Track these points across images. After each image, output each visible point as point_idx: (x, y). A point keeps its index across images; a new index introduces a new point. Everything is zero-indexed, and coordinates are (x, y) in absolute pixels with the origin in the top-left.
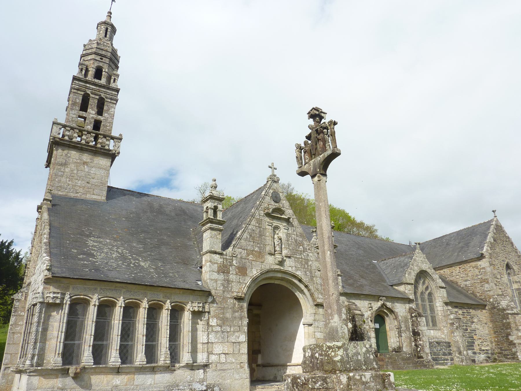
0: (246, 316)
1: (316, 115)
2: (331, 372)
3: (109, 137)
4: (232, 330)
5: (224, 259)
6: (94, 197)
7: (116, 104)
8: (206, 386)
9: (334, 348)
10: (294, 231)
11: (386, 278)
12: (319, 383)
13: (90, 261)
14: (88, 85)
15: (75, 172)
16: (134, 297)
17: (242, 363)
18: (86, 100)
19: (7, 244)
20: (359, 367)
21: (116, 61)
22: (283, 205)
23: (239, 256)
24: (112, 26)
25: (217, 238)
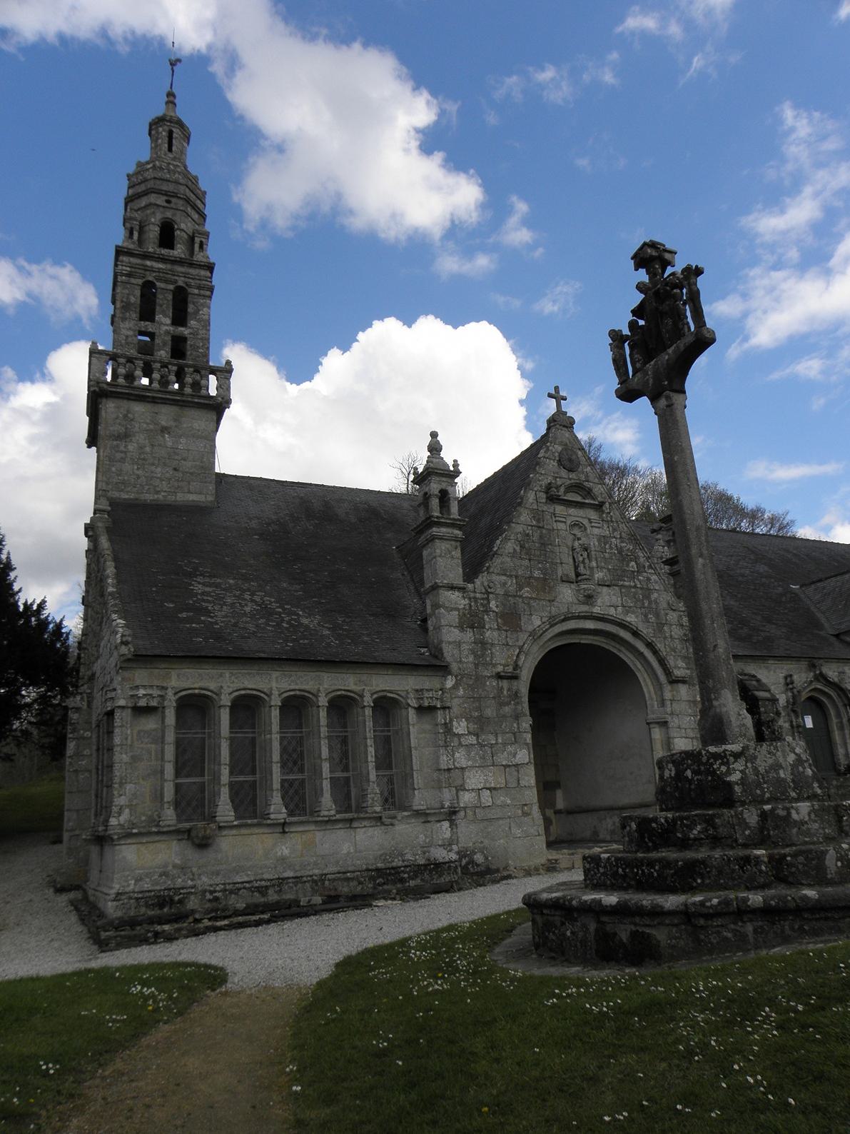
0: (528, 714)
1: (651, 257)
2: (721, 806)
3: (206, 369)
4: (500, 741)
5: (470, 599)
6: (192, 497)
7: (210, 297)
8: (458, 853)
9: (725, 756)
10: (614, 530)
11: (823, 620)
12: (699, 828)
13: (203, 622)
14: (148, 263)
15: (148, 449)
16: (297, 687)
17: (526, 805)
18: (148, 290)
19: (35, 607)
20: (783, 794)
21: (199, 203)
22: (587, 476)
23: (500, 591)
24: (180, 124)
25: (452, 557)
